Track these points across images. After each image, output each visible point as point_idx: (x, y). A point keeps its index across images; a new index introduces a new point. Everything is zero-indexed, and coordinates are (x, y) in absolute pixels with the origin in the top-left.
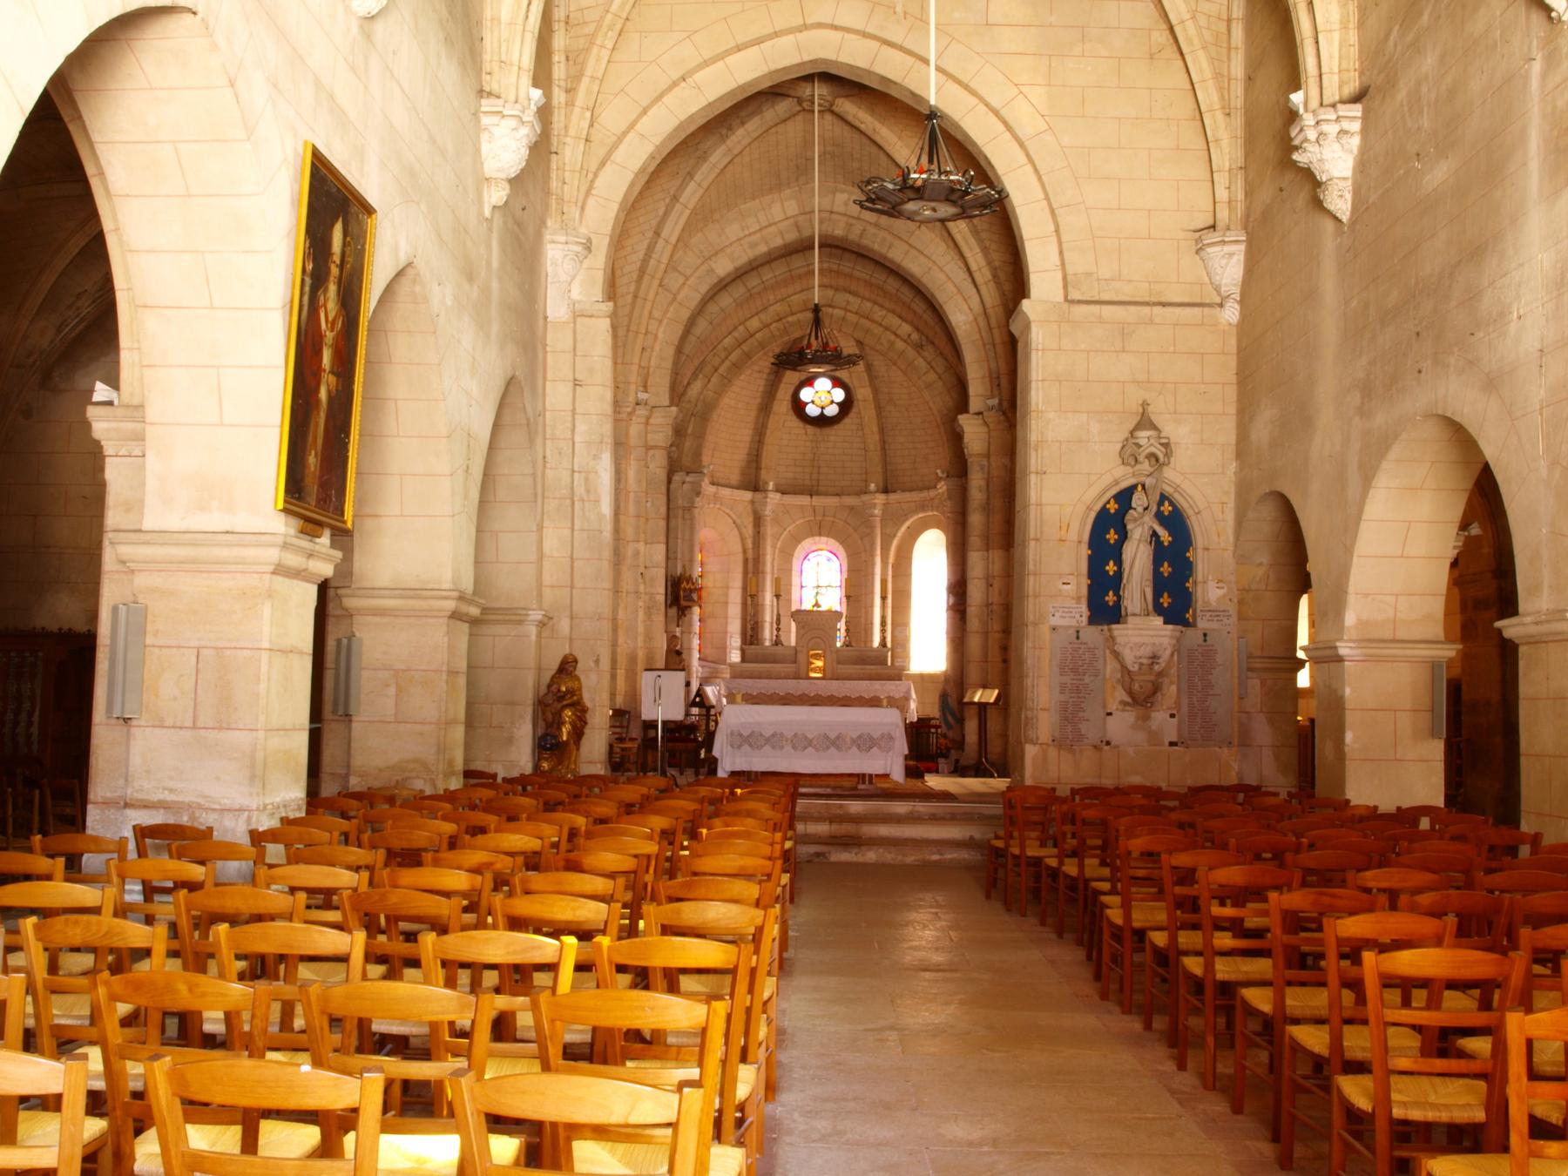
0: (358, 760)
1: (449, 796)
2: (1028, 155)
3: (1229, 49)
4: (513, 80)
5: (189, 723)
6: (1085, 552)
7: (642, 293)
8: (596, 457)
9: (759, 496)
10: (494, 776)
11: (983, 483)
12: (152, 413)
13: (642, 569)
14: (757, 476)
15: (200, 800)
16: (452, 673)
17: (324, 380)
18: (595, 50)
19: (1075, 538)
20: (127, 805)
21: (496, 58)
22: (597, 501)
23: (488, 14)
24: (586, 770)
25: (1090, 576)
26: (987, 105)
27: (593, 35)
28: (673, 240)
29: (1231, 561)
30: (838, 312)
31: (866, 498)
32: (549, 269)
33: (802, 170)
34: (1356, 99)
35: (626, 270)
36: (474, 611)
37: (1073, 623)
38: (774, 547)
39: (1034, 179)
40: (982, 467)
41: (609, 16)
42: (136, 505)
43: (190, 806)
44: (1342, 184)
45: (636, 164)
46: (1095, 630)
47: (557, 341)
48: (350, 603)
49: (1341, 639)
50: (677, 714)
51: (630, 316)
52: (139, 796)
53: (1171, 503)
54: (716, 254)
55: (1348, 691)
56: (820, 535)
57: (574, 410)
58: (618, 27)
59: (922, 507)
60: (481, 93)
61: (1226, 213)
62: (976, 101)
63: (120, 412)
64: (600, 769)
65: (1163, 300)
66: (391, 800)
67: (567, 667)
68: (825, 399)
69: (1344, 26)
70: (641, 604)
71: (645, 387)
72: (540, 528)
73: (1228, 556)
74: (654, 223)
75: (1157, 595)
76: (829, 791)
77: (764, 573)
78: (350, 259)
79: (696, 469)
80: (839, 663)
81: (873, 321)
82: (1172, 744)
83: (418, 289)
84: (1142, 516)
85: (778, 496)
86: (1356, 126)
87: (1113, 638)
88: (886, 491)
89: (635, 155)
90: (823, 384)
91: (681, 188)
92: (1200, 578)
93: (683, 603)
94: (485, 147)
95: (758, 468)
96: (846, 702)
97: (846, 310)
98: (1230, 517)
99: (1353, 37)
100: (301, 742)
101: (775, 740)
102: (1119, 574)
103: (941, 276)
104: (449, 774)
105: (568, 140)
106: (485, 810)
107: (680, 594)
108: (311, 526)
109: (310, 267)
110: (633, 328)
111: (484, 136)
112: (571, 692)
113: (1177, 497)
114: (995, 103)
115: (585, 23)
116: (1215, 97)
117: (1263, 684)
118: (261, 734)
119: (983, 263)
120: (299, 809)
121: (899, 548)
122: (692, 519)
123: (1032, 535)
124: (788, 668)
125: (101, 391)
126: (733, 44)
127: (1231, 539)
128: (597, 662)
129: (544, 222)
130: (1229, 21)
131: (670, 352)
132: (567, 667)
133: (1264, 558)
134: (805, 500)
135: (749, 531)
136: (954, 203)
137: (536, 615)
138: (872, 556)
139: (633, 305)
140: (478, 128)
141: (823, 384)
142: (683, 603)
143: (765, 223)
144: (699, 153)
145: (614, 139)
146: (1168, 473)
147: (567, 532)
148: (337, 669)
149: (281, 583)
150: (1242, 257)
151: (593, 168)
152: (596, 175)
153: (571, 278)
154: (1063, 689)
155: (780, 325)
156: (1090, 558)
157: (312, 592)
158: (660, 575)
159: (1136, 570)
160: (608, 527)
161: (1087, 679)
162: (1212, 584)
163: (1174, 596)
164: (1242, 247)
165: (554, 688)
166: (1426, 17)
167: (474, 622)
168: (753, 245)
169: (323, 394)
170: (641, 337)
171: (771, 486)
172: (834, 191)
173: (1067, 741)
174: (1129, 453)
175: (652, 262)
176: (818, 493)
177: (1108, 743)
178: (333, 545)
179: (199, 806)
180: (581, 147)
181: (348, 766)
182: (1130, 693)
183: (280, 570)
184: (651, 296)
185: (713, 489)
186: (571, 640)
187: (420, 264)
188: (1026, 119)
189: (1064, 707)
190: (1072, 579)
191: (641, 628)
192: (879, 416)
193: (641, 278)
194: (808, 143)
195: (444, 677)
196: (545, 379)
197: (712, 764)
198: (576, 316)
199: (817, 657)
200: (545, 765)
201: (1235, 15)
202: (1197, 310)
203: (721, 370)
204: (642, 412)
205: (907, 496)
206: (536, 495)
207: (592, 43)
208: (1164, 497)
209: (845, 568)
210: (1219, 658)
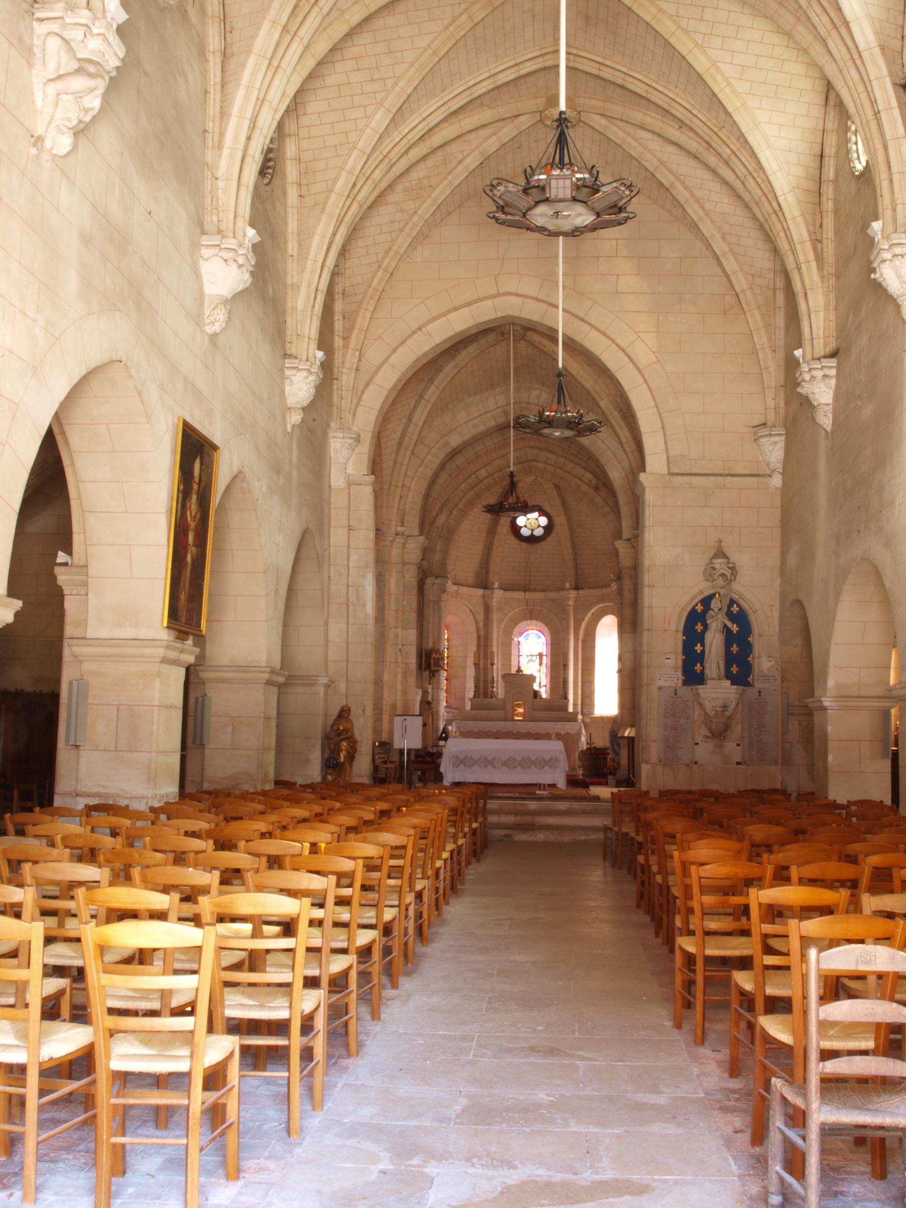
0: (209, 773)
1: (264, 793)
2: (644, 378)
3: (775, 308)
4: (305, 345)
5: (113, 748)
6: (680, 638)
8: (363, 577)
9: (488, 592)
10: (295, 784)
12: (93, 570)
13: (400, 647)
14: (487, 578)
15: (119, 792)
16: (267, 718)
17: (189, 551)
18: (362, 312)
19: (674, 629)
20: (77, 795)
21: (294, 333)
22: (364, 605)
23: (289, 305)
24: (356, 780)
25: (684, 653)
26: (617, 345)
27: (361, 302)
28: (420, 424)
30: (541, 465)
31: (562, 593)
32: (332, 455)
34: (833, 355)
36: (281, 680)
37: (673, 684)
38: (499, 628)
39: (648, 394)
41: (371, 290)
42: (83, 623)
43: (113, 795)
44: (826, 408)
45: (389, 384)
46: (687, 689)
47: (338, 501)
48: (203, 675)
49: (825, 696)
50: (417, 744)
51: (392, 474)
52: (84, 790)
53: (738, 606)
54: (450, 432)
55: (830, 729)
56: (531, 619)
57: (349, 547)
58: (377, 297)
59: (602, 599)
60: (285, 356)
61: (773, 415)
62: (610, 342)
63: (73, 570)
64: (366, 780)
65: (732, 472)
66: (229, 795)
67: (344, 714)
68: (534, 524)
69: (827, 309)
70: (399, 670)
71: (402, 522)
72: (326, 624)
75: (728, 666)
76: (517, 795)
78: (204, 479)
79: (442, 574)
80: (533, 710)
82: (738, 763)
83: (245, 485)
84: (717, 614)
85: (501, 592)
86: (833, 372)
87: (698, 694)
88: (577, 588)
89: (388, 379)
91: (426, 389)
92: (756, 654)
93: (433, 668)
94: (287, 389)
95: (487, 573)
96: (538, 736)
97: (546, 463)
98: (776, 614)
99: (832, 315)
100: (176, 759)
101: (488, 762)
102: (703, 652)
104: (265, 780)
105: (344, 370)
106: (283, 800)
107: (429, 662)
108: (182, 635)
109: (182, 487)
110: (393, 483)
111: (287, 382)
112: (346, 730)
113: (741, 602)
114: (623, 344)
115: (356, 294)
116: (765, 340)
117: (800, 724)
118: (154, 755)
120: (175, 798)
121: (586, 629)
123: (646, 627)
125: (62, 557)
126: (452, 306)
127: (777, 630)
128: (364, 710)
129: (328, 425)
130: (775, 289)
131: (419, 499)
132: (344, 714)
134: (520, 595)
135: (481, 617)
136: (572, 429)
137: (324, 680)
138: (568, 634)
140: (283, 377)
142: (433, 668)
145: (374, 369)
146: (735, 586)
147: (345, 626)
148: (196, 716)
149: (166, 668)
150: (783, 445)
151: (361, 388)
152: (363, 393)
153: (346, 460)
154: (666, 727)
156: (684, 642)
157: (183, 671)
158: (413, 650)
159: (713, 650)
160: (371, 622)
161: (682, 721)
163: (739, 667)
164: (783, 438)
165: (335, 728)
166: (863, 311)
167: (280, 686)
169: (189, 558)
170: (399, 489)
173: (669, 761)
174: (710, 573)
175: (406, 439)
176: (530, 590)
177: (696, 763)
178: (195, 645)
179: (119, 796)
180: (353, 374)
181: (203, 776)
182: (710, 730)
183: (165, 661)
184: (406, 461)
185: (455, 588)
186: (347, 696)
187: (246, 470)
188: (644, 351)
190: (672, 656)
191: (399, 687)
192: (572, 535)
195: (262, 720)
196: (329, 526)
197: (439, 777)
198: (350, 484)
199: (519, 706)
200: (330, 778)
201: (778, 286)
202: (754, 479)
203: (460, 506)
204: (400, 540)
205: (591, 591)
206: (323, 603)
207: (360, 307)
208: (732, 602)
209: (549, 643)
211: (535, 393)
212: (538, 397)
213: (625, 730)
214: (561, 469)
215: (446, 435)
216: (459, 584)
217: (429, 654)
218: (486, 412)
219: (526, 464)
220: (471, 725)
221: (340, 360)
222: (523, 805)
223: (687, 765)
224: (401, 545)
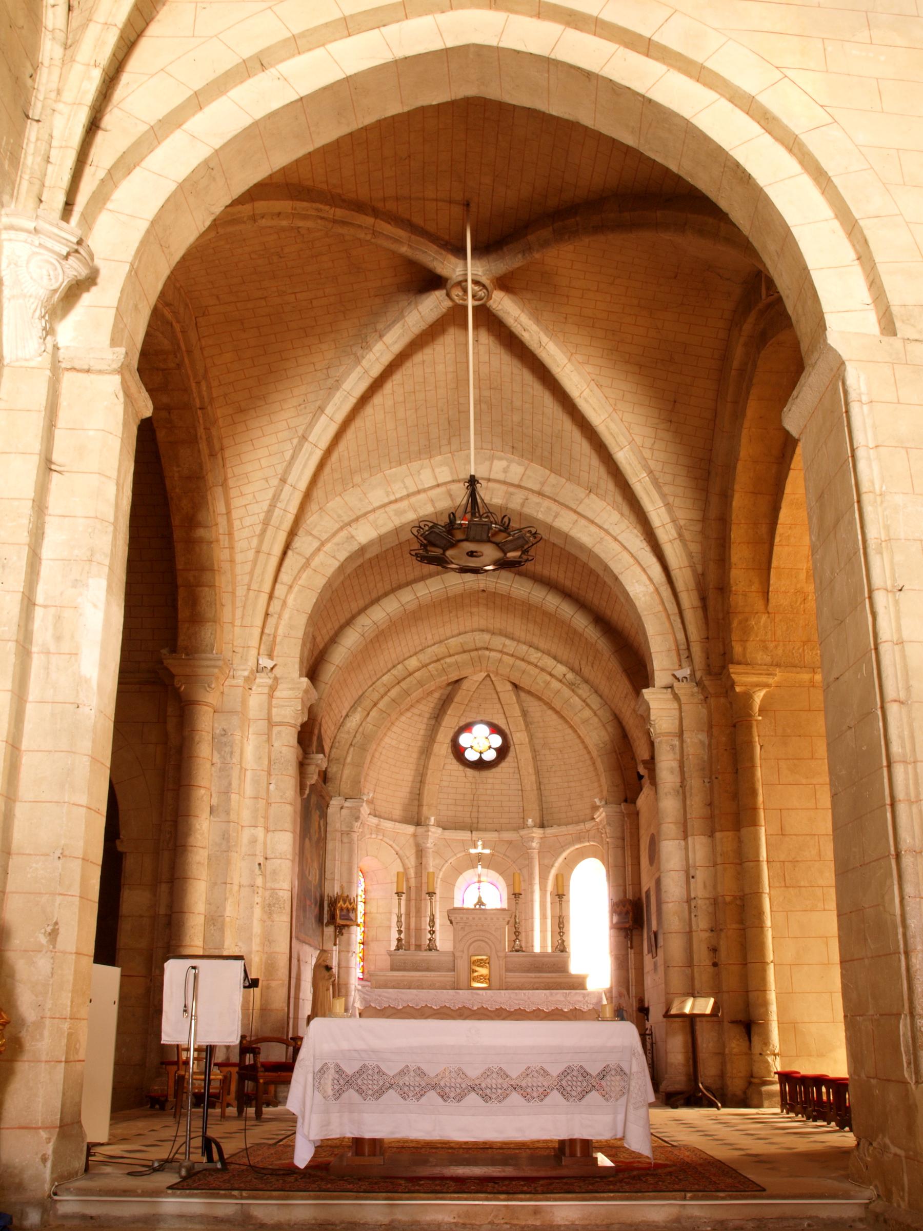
7: (265, 548)
9: (420, 830)
11: (675, 765)
13: (261, 860)
14: (419, 813)
22: (74, 654)
31: (523, 832)
33: (455, 429)
35: (248, 521)
40: (673, 747)
51: (251, 573)
54: (357, 519)
68: (483, 745)
70: (258, 899)
74: (280, 469)
80: (507, 970)
81: (529, 663)
85: (440, 830)
88: (542, 826)
90: (481, 730)
91: (311, 425)
93: (339, 921)
95: (420, 806)
96: (519, 1015)
101: (416, 1085)
103: (616, 547)
105: (60, 106)
110: (254, 586)
119: (667, 519)
122: (351, 842)
124: (448, 977)
128: (53, 934)
135: (411, 862)
138: (531, 884)
139: (255, 562)
141: (481, 730)
142: (339, 921)
143: (413, 489)
144: (330, 382)
168: (399, 513)
171: (433, 820)
172: (492, 458)
175: (277, 512)
176: (477, 829)
185: (374, 821)
191: (257, 928)
192: (534, 758)
193: (264, 531)
194: (461, 382)
199: (480, 963)
203: (381, 705)
205: (563, 829)
212: (505, 471)
213: (683, 1002)
214: (523, 660)
215: (349, 524)
216: (380, 817)
217: (333, 903)
218: (419, 492)
219: (473, 654)
220: (391, 997)
221: (54, 85)
222: (536, 1211)
224: (266, 690)
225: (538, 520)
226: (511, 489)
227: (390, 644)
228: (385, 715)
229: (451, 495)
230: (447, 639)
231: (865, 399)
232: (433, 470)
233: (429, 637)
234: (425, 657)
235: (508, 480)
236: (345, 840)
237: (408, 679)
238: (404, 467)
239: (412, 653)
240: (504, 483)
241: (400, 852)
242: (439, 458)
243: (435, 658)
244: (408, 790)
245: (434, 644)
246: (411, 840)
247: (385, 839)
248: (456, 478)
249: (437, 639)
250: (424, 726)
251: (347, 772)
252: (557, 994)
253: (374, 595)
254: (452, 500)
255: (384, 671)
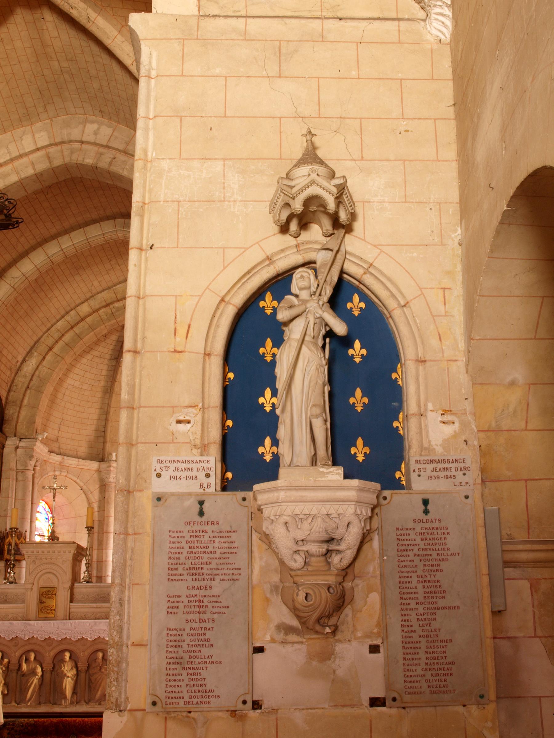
9: (104, 465)
19: (200, 348)
25: (226, 407)
29: (464, 378)
37: (194, 487)
46: (233, 498)
53: (364, 297)
73: (459, 370)
77: (107, 532)
82: (375, 702)
98: (458, 310)
117: (534, 586)
127: (462, 345)
133: (518, 372)
135: (95, 496)
143: (15, 154)
146: (352, 243)
155: (107, 310)
161: (217, 587)
162: (433, 418)
163: (366, 428)
172: (85, 122)
177: (257, 705)
182: (295, 611)
189: (175, 639)
203: (56, 349)
210: (453, 542)
211: (91, 128)
212: (96, 133)
218: (21, 156)
223: (233, 713)
225: (123, 177)
226: (102, 150)
227: (56, 292)
228: (59, 358)
229: (49, 158)
230: (115, 286)
231: (153, 74)
232: (34, 135)
233: (96, 283)
234: (95, 303)
235: (97, 142)
236: (20, 478)
237: (81, 324)
238: (9, 134)
239: (83, 300)
240: (95, 144)
241: (85, 488)
242: (39, 124)
243: (104, 304)
244: (94, 427)
245: (103, 290)
246: (96, 476)
247: (69, 476)
248: (53, 142)
249: (104, 285)
250: (105, 367)
251: (23, 414)
252: (101, 623)
253: (20, 249)
254: (50, 162)
255: (58, 317)
